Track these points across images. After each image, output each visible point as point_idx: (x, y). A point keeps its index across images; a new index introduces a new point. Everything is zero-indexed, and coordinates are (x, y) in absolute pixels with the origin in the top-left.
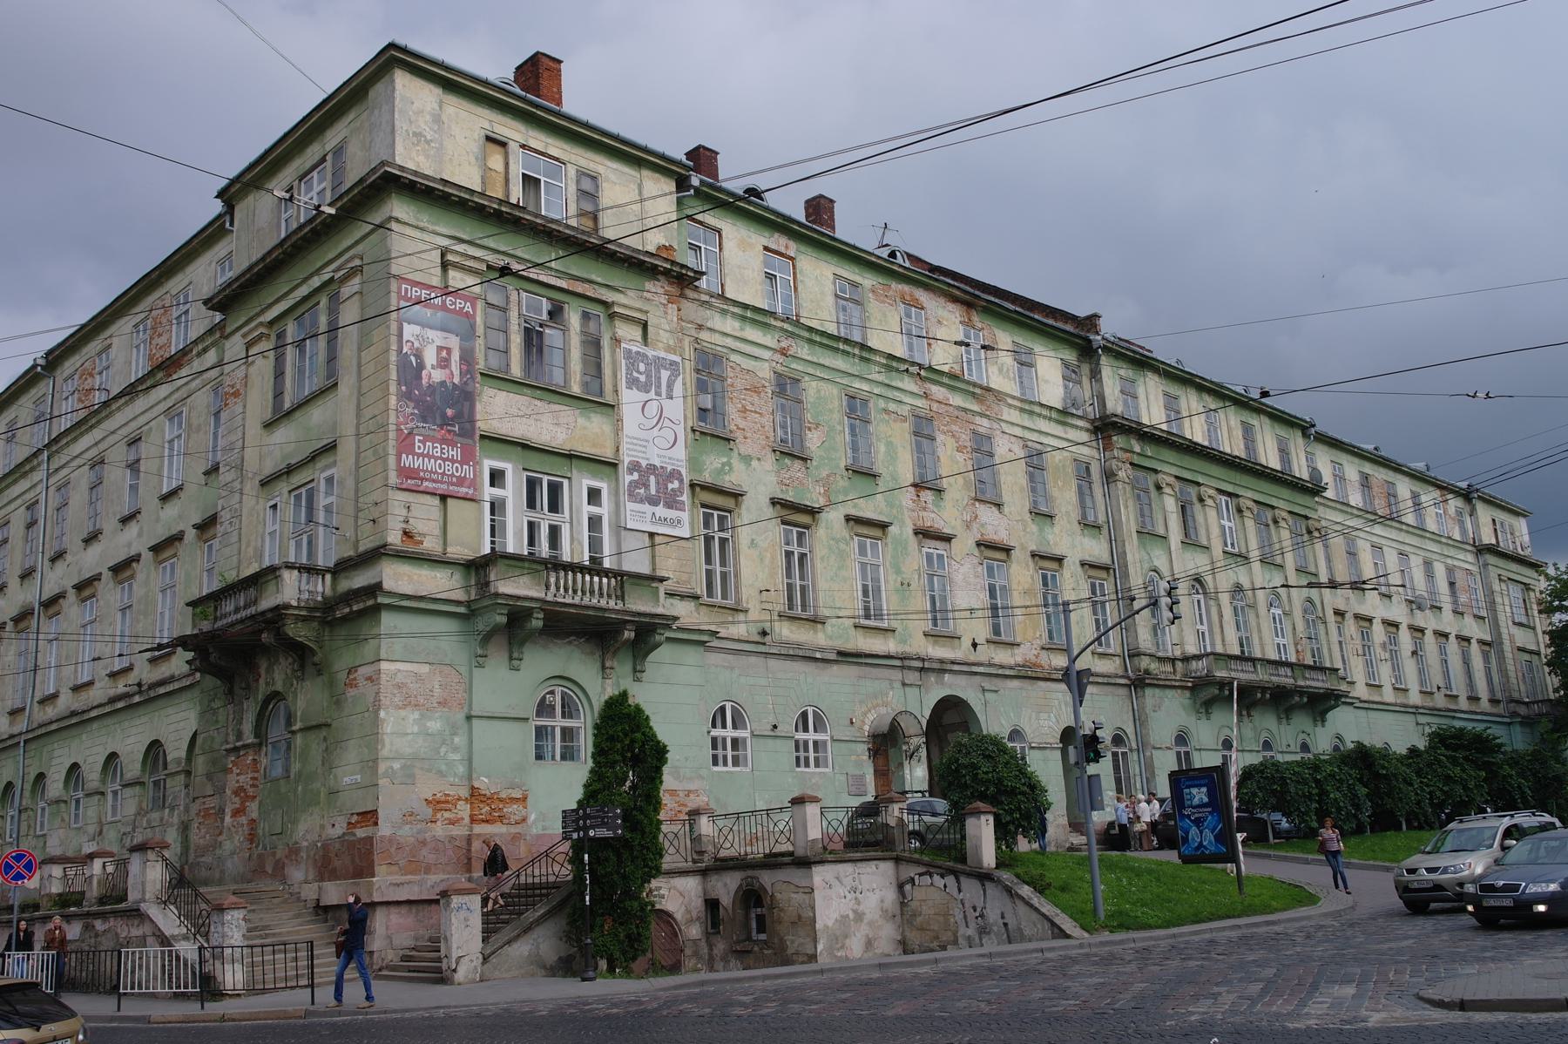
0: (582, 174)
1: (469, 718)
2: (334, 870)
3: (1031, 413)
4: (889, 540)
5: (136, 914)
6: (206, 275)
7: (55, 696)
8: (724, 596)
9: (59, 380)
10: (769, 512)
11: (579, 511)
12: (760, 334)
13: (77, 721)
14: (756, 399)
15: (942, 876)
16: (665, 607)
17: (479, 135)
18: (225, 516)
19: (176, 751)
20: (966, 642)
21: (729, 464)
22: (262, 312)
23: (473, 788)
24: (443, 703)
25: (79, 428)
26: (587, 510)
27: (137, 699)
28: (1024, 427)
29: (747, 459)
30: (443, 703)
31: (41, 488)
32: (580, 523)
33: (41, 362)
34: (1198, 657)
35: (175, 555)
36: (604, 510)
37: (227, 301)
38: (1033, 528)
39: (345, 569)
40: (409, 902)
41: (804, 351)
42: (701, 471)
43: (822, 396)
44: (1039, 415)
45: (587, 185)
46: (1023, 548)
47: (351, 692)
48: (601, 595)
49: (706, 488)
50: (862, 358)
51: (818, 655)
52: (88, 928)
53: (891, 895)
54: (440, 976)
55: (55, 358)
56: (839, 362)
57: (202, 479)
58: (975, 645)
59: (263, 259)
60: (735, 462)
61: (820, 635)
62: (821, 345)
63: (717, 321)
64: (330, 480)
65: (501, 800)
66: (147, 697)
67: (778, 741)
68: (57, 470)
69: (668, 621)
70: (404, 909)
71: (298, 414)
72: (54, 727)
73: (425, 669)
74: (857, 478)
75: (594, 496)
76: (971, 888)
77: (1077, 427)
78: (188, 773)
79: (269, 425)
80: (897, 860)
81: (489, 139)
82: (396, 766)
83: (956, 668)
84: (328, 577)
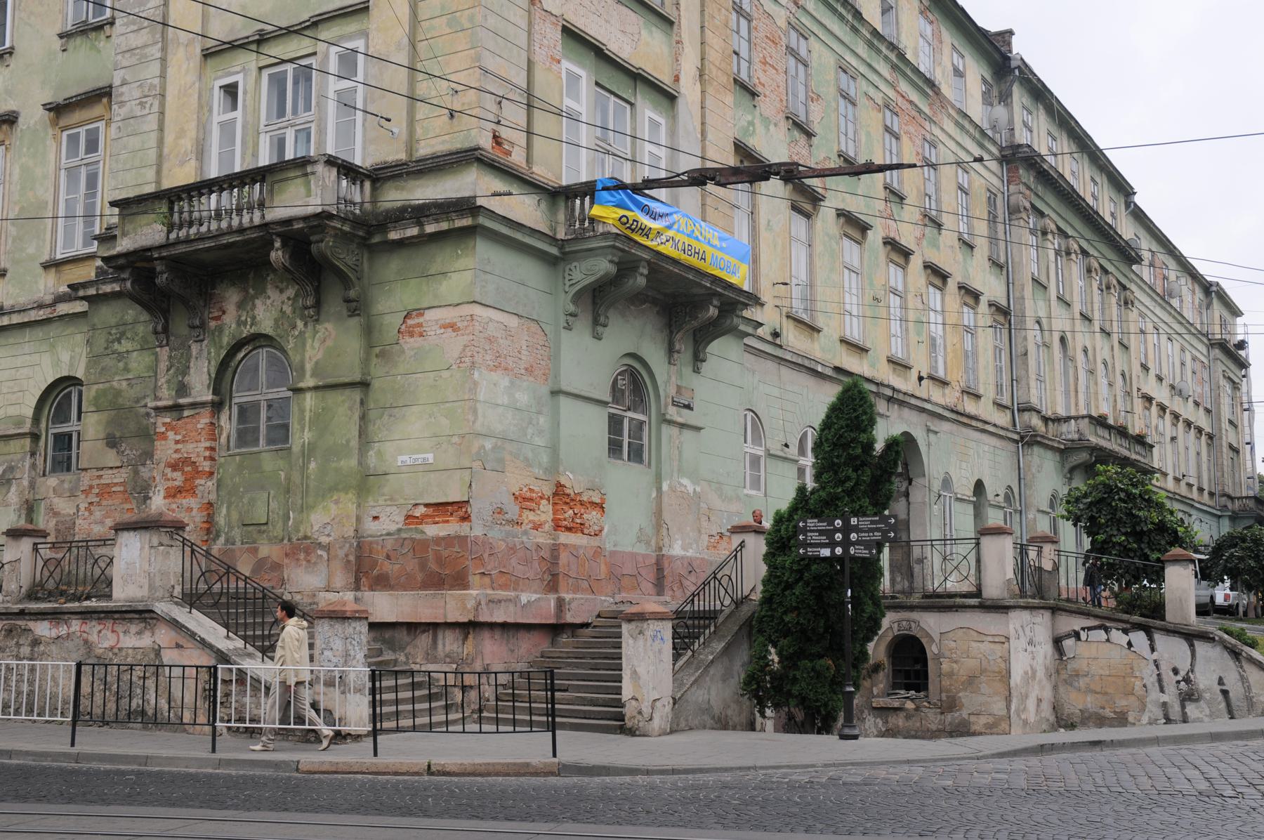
1: (555, 393)
3: (962, 128)
4: (866, 245)
15: (1125, 632)
18: (128, 94)
21: (751, 123)
23: (559, 485)
24: (529, 370)
28: (958, 143)
29: (766, 121)
30: (529, 370)
40: (504, 626)
44: (967, 132)
47: (409, 343)
51: (820, 369)
53: (1045, 649)
57: (58, 43)
58: (921, 379)
61: (816, 346)
64: (348, 60)
65: (582, 503)
70: (497, 634)
73: (513, 322)
76: (1172, 650)
78: (35, 437)
80: (1054, 610)
82: (488, 445)
83: (913, 401)
84: (367, 185)
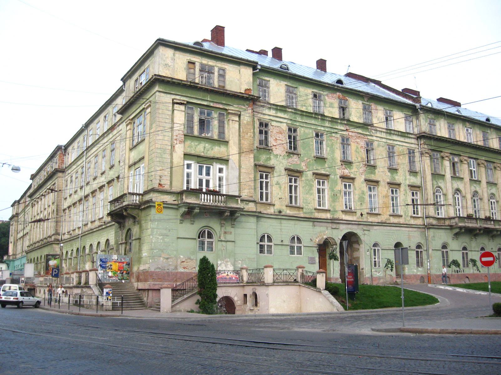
0: (220, 69)
2: (141, 280)
4: (330, 180)
5: (89, 287)
6: (121, 102)
7: (87, 224)
8: (267, 199)
9: (88, 131)
10: (283, 172)
11: (216, 175)
12: (283, 114)
13: (92, 232)
14: (280, 136)
16: (240, 205)
17: (185, 62)
19: (112, 242)
20: (359, 214)
22: (129, 116)
25: (93, 145)
26: (218, 175)
27: (104, 227)
31: (84, 163)
32: (215, 179)
33: (84, 126)
34: (454, 218)
35: (112, 186)
36: (224, 175)
37: (123, 111)
38: (389, 174)
39: (146, 194)
41: (299, 119)
42: (259, 161)
43: (305, 132)
45: (221, 72)
46: (384, 181)
48: (219, 202)
49: (260, 166)
50: (322, 119)
52: (82, 290)
54: (158, 309)
55: (87, 125)
56: (313, 121)
57: (109, 169)
58: (362, 215)
59: (129, 101)
60: (272, 157)
62: (306, 116)
63: (267, 111)
66: (102, 228)
67: (283, 247)
68: (88, 158)
69: (241, 210)
71: (138, 146)
72: (87, 233)
74: (318, 160)
75: (221, 170)
77: (411, 138)
79: (131, 150)
81: (189, 62)
